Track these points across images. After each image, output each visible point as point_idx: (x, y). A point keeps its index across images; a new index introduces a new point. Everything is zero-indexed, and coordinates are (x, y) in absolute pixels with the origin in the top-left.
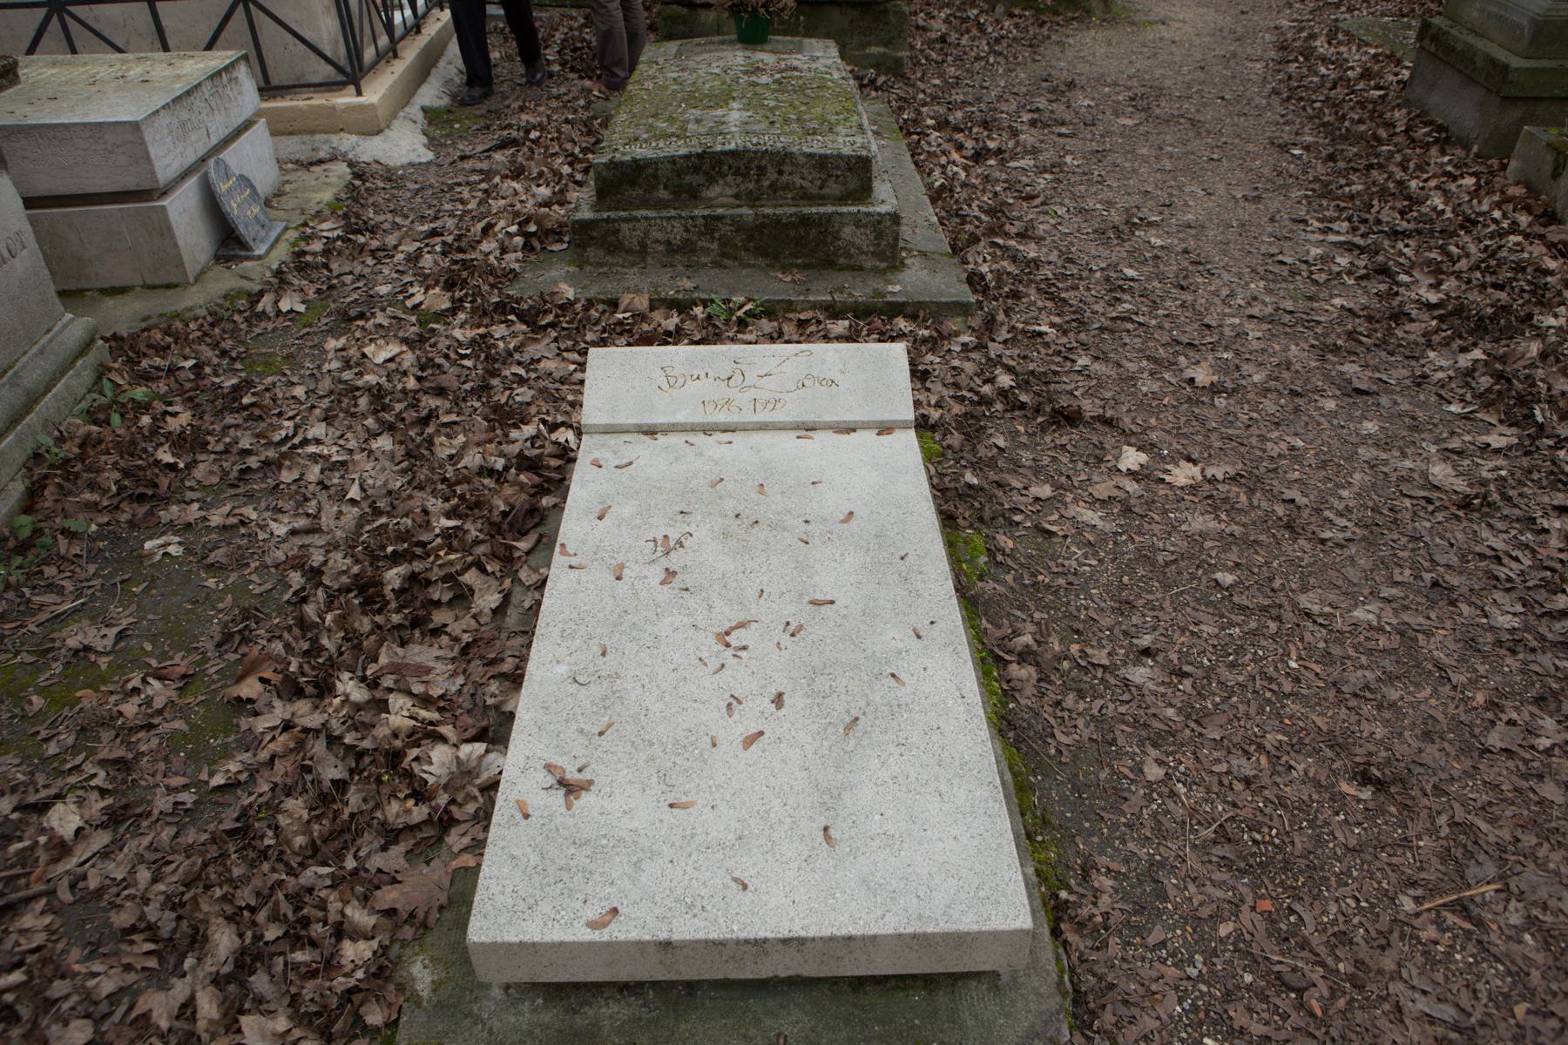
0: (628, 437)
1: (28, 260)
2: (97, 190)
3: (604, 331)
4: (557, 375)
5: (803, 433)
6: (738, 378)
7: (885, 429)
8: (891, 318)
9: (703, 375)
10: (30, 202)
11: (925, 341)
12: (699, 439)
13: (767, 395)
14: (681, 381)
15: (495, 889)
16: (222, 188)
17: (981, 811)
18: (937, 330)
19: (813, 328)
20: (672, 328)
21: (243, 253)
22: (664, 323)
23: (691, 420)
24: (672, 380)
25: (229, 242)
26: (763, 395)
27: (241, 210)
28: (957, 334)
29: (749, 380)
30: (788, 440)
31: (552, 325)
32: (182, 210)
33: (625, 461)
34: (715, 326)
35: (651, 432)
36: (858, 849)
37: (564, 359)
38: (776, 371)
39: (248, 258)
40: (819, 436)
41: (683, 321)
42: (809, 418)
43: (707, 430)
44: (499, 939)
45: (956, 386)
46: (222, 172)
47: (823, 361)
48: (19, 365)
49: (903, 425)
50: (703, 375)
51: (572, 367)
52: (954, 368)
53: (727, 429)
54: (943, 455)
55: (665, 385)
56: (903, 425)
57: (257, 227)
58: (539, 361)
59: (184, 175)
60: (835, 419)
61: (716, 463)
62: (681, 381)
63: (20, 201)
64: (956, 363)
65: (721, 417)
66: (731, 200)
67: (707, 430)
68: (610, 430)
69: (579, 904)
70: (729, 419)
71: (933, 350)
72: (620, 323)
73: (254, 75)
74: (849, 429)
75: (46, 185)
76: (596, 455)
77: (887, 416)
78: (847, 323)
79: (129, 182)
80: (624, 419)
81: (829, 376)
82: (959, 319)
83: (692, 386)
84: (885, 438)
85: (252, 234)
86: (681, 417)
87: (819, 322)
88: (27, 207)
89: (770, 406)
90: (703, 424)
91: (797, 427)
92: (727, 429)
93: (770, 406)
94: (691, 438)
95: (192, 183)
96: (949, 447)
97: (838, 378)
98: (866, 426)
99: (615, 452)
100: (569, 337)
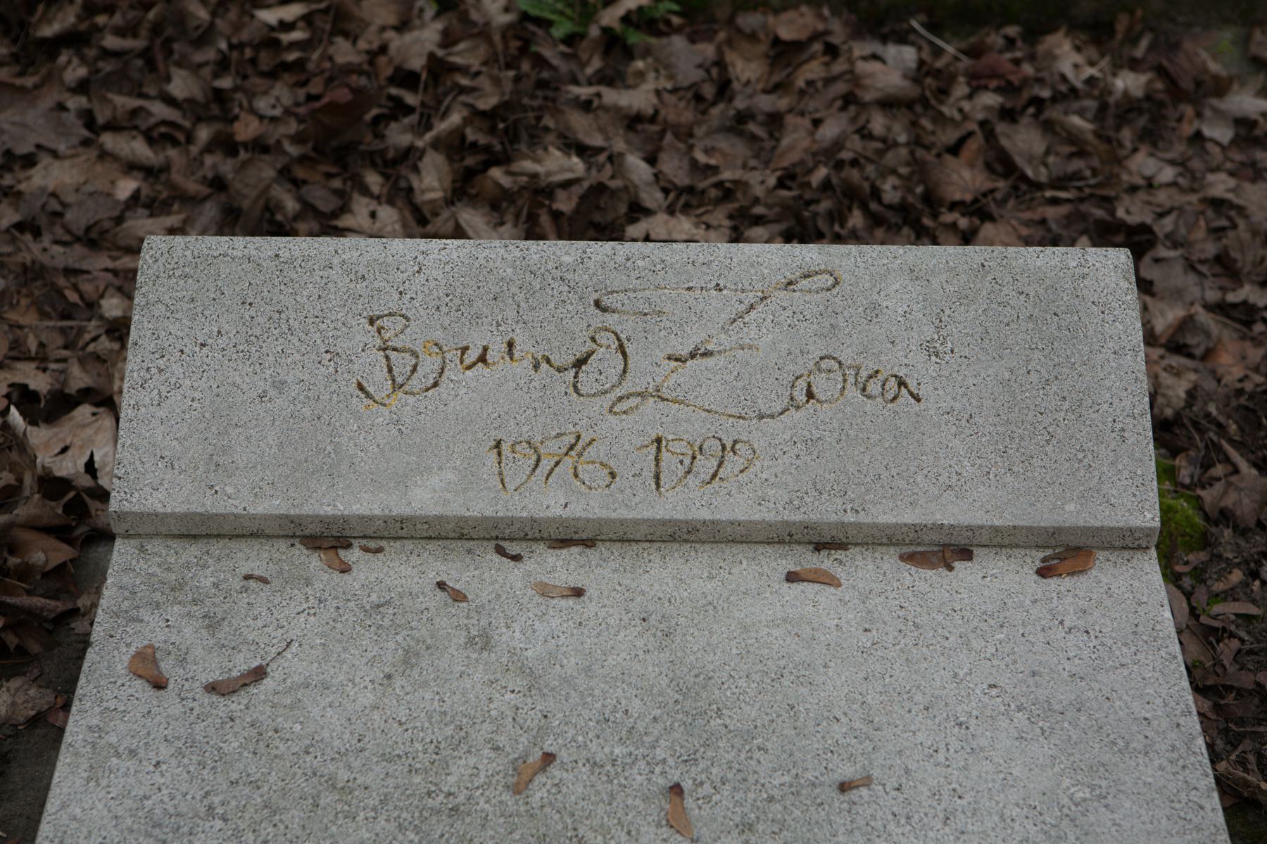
0: (253, 558)
3: (223, 65)
4: (77, 218)
5: (810, 560)
6: (606, 361)
7: (1065, 554)
8: (1034, 33)
9: (497, 352)
11: (1129, 108)
12: (483, 575)
13: (694, 427)
14: (429, 366)
18: (1161, 71)
19: (813, 70)
20: (417, 63)
22: (396, 42)
23: (456, 509)
24: (402, 363)
26: (687, 426)
28: (1220, 88)
29: (648, 367)
30: (755, 579)
31: (74, 40)
33: (243, 663)
34: (540, 62)
35: (330, 539)
37: (104, 155)
38: (727, 325)
40: (863, 572)
41: (448, 40)
42: (826, 511)
43: (506, 539)
45: (1225, 266)
47: (875, 310)
49: (1125, 542)
50: (497, 352)
51: (126, 187)
52: (1217, 204)
53: (570, 538)
54: (1205, 542)
55: (378, 382)
56: (1125, 542)
58: (29, 161)
60: (909, 517)
61: (534, 683)
62: (429, 366)
64: (1220, 185)
65: (552, 502)
67: (506, 539)
68: (200, 530)
70: (577, 510)
71: (1151, 137)
72: (269, 41)
74: (946, 550)
76: (152, 631)
77: (1072, 513)
78: (909, 54)
80: (239, 498)
81: (892, 362)
82: (1226, 37)
83: (465, 386)
84: (1068, 592)
86: (426, 497)
87: (832, 51)
89: (706, 466)
90: (495, 523)
91: (782, 537)
92: (570, 538)
93: (706, 466)
94: (459, 572)
96: (1225, 517)
97: (921, 372)
98: (1005, 540)
99: (212, 622)
100: (121, 81)
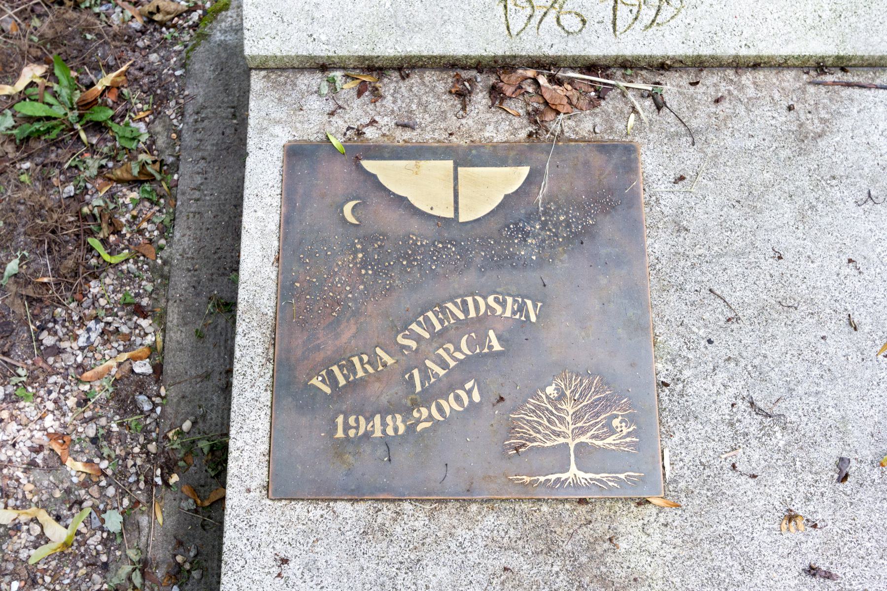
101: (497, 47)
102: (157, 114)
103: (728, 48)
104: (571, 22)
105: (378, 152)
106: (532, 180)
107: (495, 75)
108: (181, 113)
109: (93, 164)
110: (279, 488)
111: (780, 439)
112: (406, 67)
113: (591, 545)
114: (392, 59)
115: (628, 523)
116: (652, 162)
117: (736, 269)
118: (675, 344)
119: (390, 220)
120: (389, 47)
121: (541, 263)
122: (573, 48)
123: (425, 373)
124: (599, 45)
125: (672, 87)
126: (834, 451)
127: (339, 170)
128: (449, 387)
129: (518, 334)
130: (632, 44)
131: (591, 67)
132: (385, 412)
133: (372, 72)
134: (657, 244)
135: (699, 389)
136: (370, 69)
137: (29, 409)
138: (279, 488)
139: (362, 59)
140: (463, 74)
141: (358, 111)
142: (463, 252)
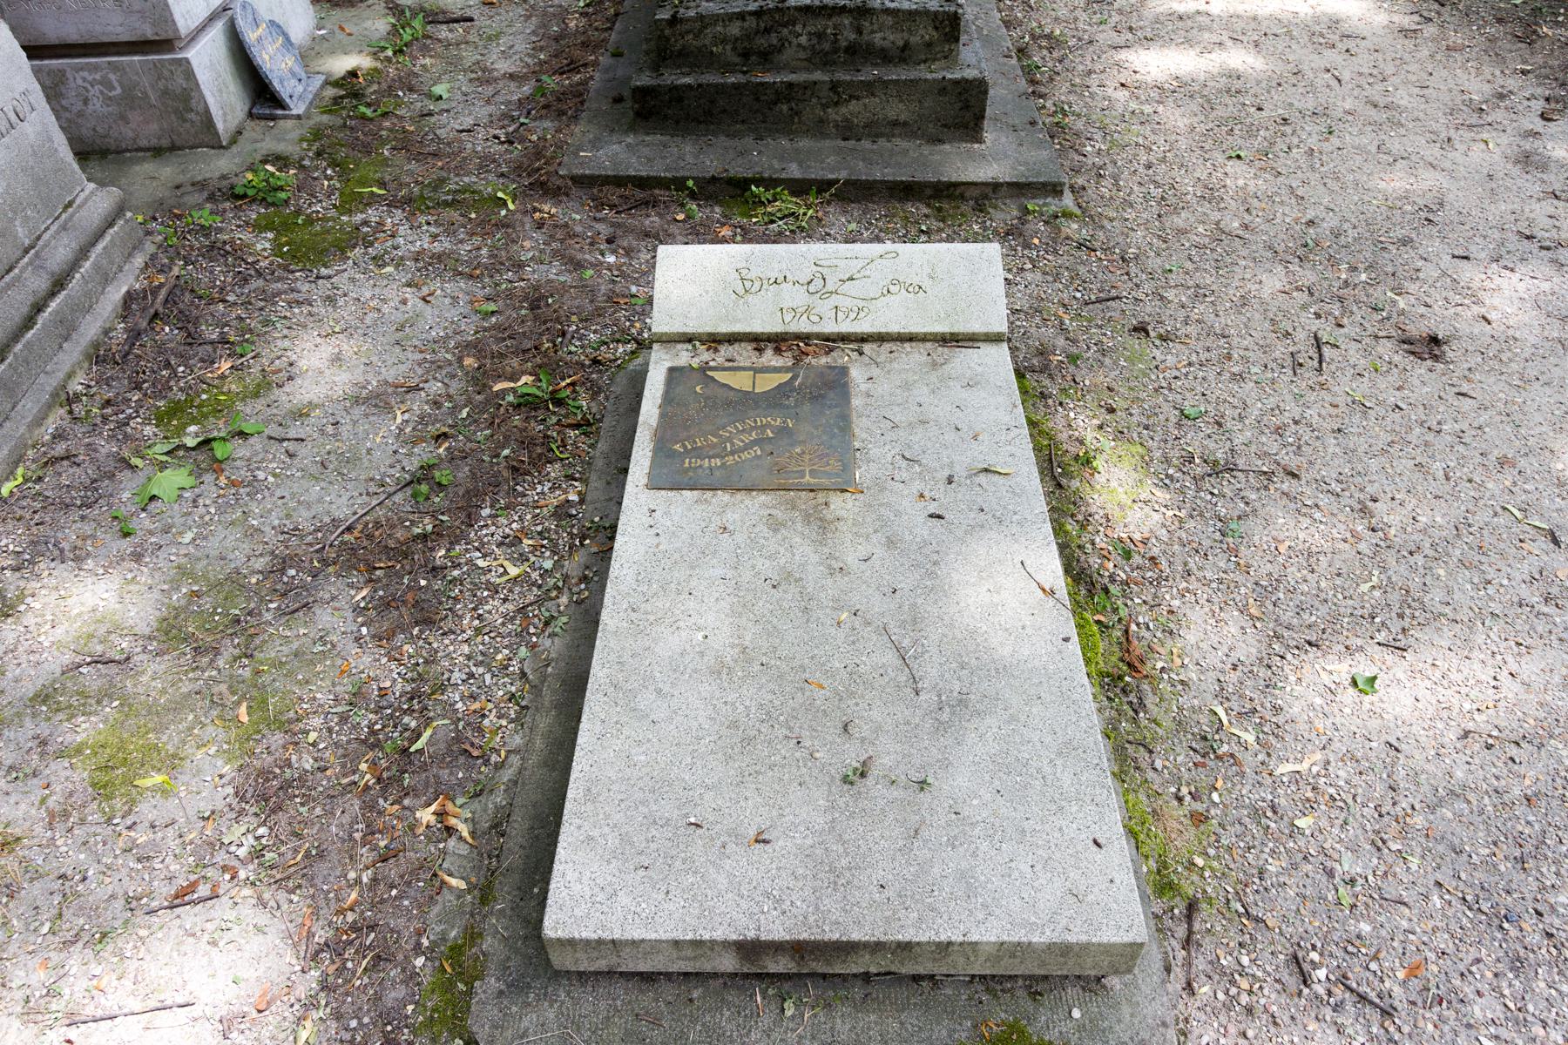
1: (42, 124)
2: (113, 39)
6: (818, 283)
10: (34, 51)
14: (757, 285)
15: (570, 876)
16: (250, 36)
17: (1088, 799)
21: (280, 112)
25: (261, 93)
27: (275, 63)
32: (207, 59)
36: (955, 838)
39: (285, 117)
44: (577, 936)
46: (250, 17)
48: (41, 243)
49: (994, 339)
56: (994, 339)
57: (294, 82)
59: (212, 19)
63: (24, 54)
66: (805, 64)
69: (661, 896)
73: (144, 159)
75: (55, 29)
79: (149, 33)
81: (916, 281)
85: (289, 90)
88: (29, 57)
95: (217, 32)
97: (926, 284)
101: (779, 329)
102: (593, 399)
103: (894, 328)
104: (815, 319)
105: (712, 369)
106: (794, 378)
107: (778, 341)
108: (607, 398)
109: (554, 419)
110: (654, 485)
111: (917, 468)
112: (733, 339)
113: (816, 507)
114: (725, 335)
115: (836, 501)
116: (857, 374)
117: (897, 409)
118: (864, 435)
119: (720, 392)
120: (724, 328)
121: (796, 406)
122: (816, 329)
123: (733, 444)
124: (829, 328)
125: (867, 348)
126: (946, 473)
127: (696, 376)
128: (746, 448)
129: (783, 431)
130: (845, 327)
131: (827, 338)
132: (710, 458)
133: (714, 341)
134: (856, 402)
135: (875, 452)
136: (714, 341)
137: (503, 521)
138: (654, 485)
139: (710, 334)
140: (759, 341)
141: (706, 356)
142: (756, 403)
